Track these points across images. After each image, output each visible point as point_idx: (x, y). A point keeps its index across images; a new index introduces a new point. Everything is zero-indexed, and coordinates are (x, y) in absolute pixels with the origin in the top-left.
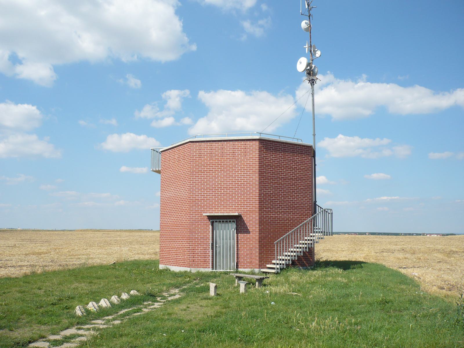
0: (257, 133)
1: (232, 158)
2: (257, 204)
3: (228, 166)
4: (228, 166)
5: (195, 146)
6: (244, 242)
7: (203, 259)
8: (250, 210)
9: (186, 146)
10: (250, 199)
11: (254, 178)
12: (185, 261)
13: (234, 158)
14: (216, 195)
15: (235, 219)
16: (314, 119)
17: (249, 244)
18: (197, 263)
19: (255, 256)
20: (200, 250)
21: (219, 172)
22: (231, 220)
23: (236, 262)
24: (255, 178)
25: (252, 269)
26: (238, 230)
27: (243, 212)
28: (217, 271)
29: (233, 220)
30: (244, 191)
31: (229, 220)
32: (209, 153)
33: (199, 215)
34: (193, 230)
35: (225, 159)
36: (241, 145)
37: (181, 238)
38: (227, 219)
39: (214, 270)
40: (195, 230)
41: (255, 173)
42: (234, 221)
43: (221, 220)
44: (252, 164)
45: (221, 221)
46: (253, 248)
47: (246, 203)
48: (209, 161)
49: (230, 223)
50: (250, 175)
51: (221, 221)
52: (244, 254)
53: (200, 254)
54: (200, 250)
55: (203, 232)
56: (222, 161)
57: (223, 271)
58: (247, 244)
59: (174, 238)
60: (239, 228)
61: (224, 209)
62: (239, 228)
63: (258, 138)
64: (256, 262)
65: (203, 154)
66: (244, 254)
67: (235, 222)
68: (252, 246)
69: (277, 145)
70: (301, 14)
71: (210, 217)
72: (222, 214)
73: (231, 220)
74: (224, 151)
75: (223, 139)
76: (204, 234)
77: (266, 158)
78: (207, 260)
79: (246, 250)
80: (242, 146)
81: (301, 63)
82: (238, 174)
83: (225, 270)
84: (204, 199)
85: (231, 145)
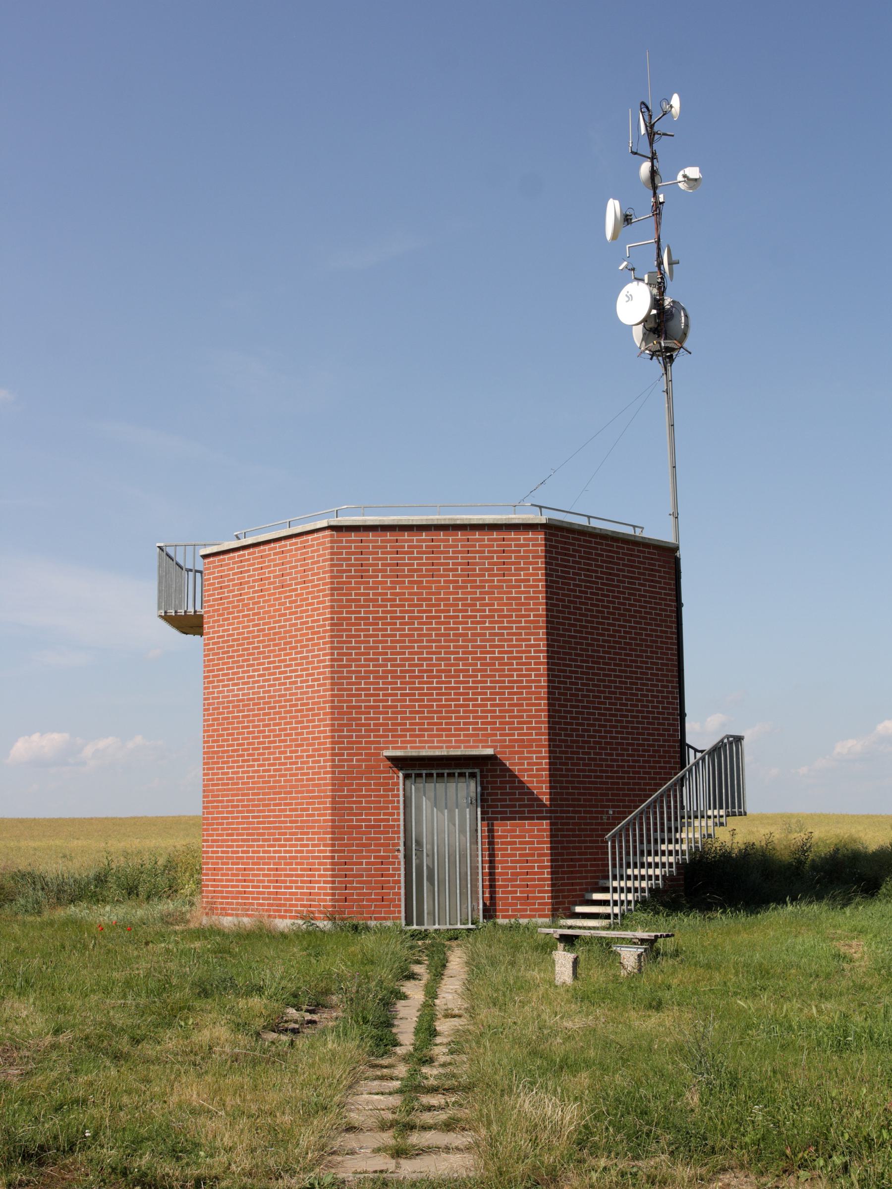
0: (532, 505)
1: (463, 581)
2: (543, 722)
3: (452, 605)
4: (452, 605)
5: (347, 542)
6: (506, 837)
7: (376, 894)
8: (523, 740)
9: (313, 540)
10: (522, 705)
11: (532, 642)
12: (217, 886)
13: (505, 581)
14: (414, 695)
15: (475, 766)
16: (675, 467)
17: (520, 843)
18: (375, 905)
19: (539, 879)
20: (367, 864)
21: (424, 623)
22: (463, 771)
23: (484, 904)
24: (539, 639)
25: (513, 920)
26: (487, 800)
27: (501, 747)
28: (423, 928)
29: (470, 771)
30: (504, 682)
31: (459, 771)
32: (389, 565)
33: (361, 754)
34: (344, 802)
35: (475, 581)
36: (382, 541)
37: (297, 828)
38: (448, 766)
39: (415, 927)
40: (349, 802)
41: (535, 628)
42: (472, 775)
43: (434, 772)
44: (526, 598)
45: (435, 775)
46: (533, 855)
47: (510, 717)
48: (390, 588)
49: (462, 779)
50: (520, 634)
51: (435, 775)
52: (507, 874)
53: (368, 876)
54: (367, 864)
55: (375, 808)
56: (431, 588)
57: (443, 927)
58: (515, 843)
59: (264, 828)
60: (489, 795)
61: (441, 736)
62: (489, 795)
63: (545, 522)
64: (544, 898)
65: (371, 565)
66: (507, 874)
67: (479, 778)
68: (530, 849)
69: (590, 542)
70: (632, 152)
71: (399, 763)
72: (437, 753)
73: (463, 771)
74: (439, 558)
75: (435, 523)
76: (379, 814)
77: (563, 583)
78: (389, 894)
79: (512, 861)
80: (493, 546)
81: (630, 298)
82: (481, 628)
83: (448, 927)
84: (378, 707)
85: (460, 540)
